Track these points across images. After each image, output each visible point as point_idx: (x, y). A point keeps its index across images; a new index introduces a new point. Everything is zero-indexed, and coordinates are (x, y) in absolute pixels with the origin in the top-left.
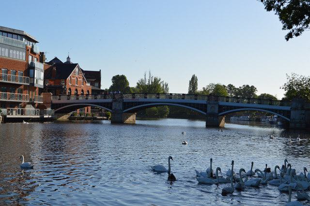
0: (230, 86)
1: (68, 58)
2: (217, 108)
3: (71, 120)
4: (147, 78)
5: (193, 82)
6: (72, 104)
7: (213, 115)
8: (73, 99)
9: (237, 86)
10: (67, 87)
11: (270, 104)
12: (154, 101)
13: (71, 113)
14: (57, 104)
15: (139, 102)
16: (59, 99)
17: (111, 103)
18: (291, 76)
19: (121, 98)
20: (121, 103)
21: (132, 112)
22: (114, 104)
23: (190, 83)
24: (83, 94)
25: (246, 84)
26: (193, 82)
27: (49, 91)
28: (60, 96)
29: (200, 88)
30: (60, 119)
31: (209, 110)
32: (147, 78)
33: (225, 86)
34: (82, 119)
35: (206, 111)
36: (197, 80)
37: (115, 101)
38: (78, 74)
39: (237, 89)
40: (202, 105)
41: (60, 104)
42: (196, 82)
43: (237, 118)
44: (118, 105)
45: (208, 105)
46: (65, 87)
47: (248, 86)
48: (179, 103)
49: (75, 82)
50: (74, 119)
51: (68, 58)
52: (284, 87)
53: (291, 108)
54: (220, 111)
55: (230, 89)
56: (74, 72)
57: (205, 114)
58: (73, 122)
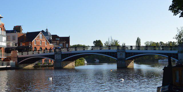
0: (161, 43)
1: (47, 29)
2: (124, 54)
3: (36, 67)
4: (110, 40)
5: (138, 41)
6: (30, 57)
7: (121, 59)
8: (36, 53)
9: (165, 43)
10: (33, 46)
11: (170, 50)
12: (82, 52)
13: (35, 64)
14: (21, 58)
15: (72, 54)
16: (28, 54)
17: (54, 55)
18: (180, 29)
19: (60, 51)
20: (60, 55)
21: (132, 59)
22: (55, 56)
23: (136, 42)
24: (36, 50)
25: (170, 41)
26: (138, 41)
27: (16, 50)
28: (28, 52)
29: (143, 44)
30: (27, 67)
31: (119, 57)
32: (110, 40)
33: (158, 43)
34: (46, 66)
35: (116, 57)
36: (140, 40)
37: (56, 54)
38: (42, 38)
39: (165, 44)
40: (113, 53)
41: (23, 58)
42: (140, 41)
43: (162, 60)
44: (58, 56)
45: (118, 53)
46: (31, 47)
47: (171, 42)
48: (98, 53)
49: (39, 42)
50: (39, 67)
51: (47, 29)
52: (176, 37)
53: (178, 52)
54: (126, 57)
55: (161, 44)
56: (39, 37)
57: (116, 59)
58: (36, 69)
